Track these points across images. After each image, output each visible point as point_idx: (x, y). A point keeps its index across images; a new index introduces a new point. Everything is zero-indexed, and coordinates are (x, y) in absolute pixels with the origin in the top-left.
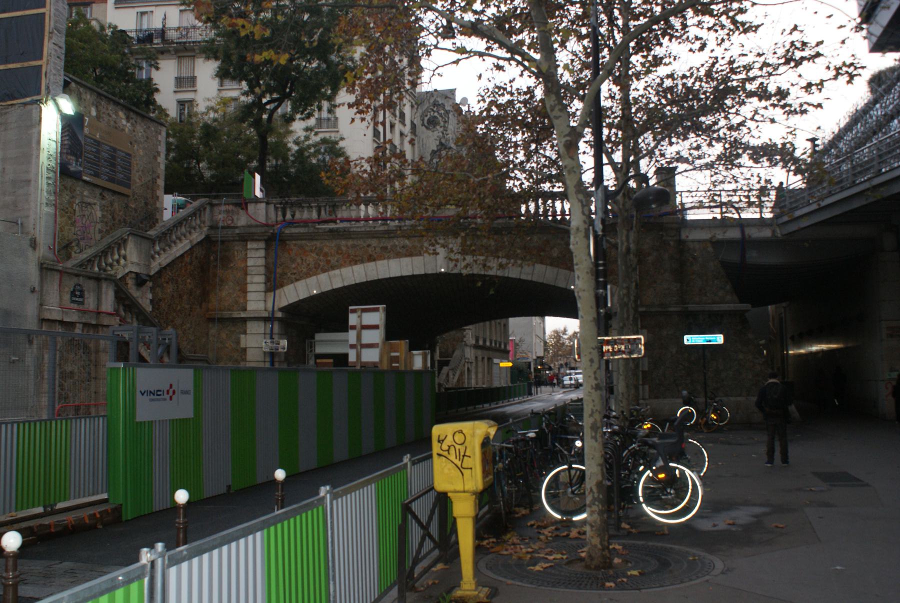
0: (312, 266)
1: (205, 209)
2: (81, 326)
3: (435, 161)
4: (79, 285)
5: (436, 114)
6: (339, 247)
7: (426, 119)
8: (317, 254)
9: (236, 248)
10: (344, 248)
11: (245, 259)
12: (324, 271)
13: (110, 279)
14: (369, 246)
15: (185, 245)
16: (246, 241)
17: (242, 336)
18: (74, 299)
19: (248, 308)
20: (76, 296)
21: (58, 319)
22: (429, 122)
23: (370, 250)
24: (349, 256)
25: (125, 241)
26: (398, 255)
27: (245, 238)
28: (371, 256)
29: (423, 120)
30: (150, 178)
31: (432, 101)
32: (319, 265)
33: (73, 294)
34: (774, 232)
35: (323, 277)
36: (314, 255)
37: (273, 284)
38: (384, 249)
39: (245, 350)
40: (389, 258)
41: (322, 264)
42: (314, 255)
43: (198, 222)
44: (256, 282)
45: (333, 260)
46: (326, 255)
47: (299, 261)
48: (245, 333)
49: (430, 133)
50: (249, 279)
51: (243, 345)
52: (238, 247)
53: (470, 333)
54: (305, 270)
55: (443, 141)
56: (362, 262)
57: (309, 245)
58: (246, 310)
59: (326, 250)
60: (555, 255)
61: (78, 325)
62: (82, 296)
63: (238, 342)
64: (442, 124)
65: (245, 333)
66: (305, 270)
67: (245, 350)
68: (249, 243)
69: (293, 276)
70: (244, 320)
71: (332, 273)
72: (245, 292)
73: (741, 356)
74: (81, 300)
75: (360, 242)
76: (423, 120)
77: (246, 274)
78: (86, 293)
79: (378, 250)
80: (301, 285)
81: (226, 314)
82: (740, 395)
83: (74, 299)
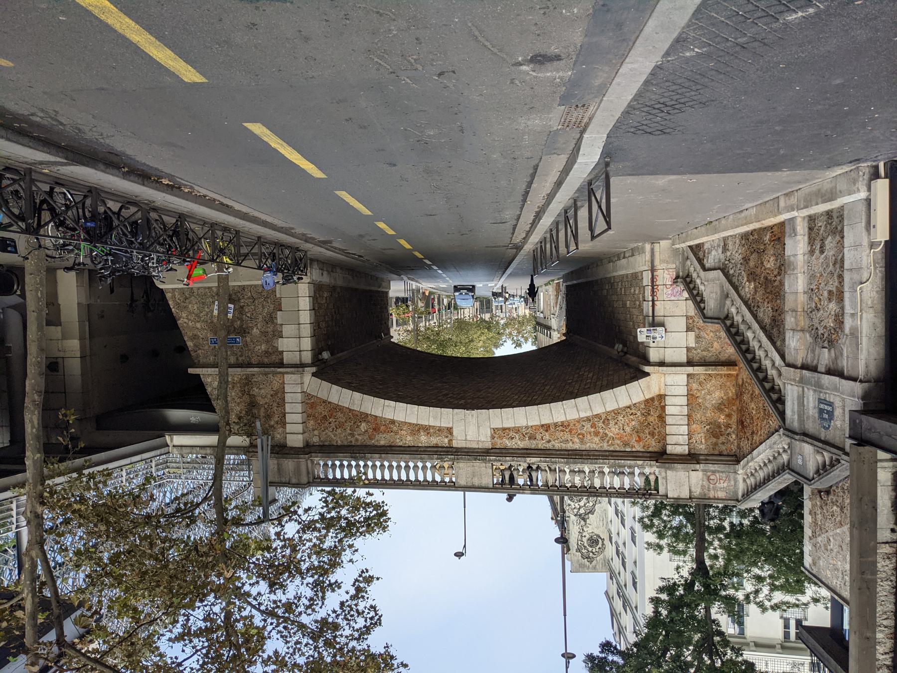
0: (612, 423)
1: (743, 496)
2: (819, 370)
3: (591, 504)
4: (824, 427)
5: (590, 549)
6: (582, 442)
7: (600, 545)
8: (606, 435)
9: (703, 447)
10: (576, 440)
11: (690, 435)
12: (598, 416)
13: (791, 432)
14: (549, 441)
15: (759, 454)
16: (689, 454)
17: (692, 344)
18: (829, 408)
19: (685, 376)
20: (828, 412)
21: (843, 381)
22: (597, 542)
23: (547, 437)
24: (570, 431)
25: (817, 472)
26: (517, 430)
27: (691, 458)
28: (547, 431)
29: (603, 544)
30: (819, 539)
31: (594, 562)
32: (604, 422)
33: (831, 414)
34: (172, 440)
35: (598, 410)
36: (610, 434)
37: (657, 404)
38: (532, 437)
39: (688, 329)
40: (527, 427)
41: (601, 424)
42: (610, 434)
43: (748, 481)
44: (676, 408)
45: (588, 426)
46: (596, 434)
47: (628, 429)
48: (688, 349)
49: (597, 532)
50: (685, 410)
51: (692, 335)
52: (702, 447)
53: (556, 337)
54: (620, 418)
55: (583, 523)
56: (556, 425)
57: (618, 446)
58: (688, 375)
59: (597, 439)
60: (363, 424)
61: (823, 370)
62: (821, 411)
63: (698, 337)
64: (585, 539)
65: (688, 349)
66: (620, 418)
67: (688, 329)
68: (687, 452)
69: (633, 411)
70: (690, 363)
71: (589, 414)
72: (690, 396)
73: (198, 325)
74: (822, 406)
75: (558, 445)
76: (603, 544)
77: (689, 416)
78: (817, 415)
79: (538, 436)
80: (624, 402)
81: (711, 371)
82: (199, 289)
83: (829, 408)
